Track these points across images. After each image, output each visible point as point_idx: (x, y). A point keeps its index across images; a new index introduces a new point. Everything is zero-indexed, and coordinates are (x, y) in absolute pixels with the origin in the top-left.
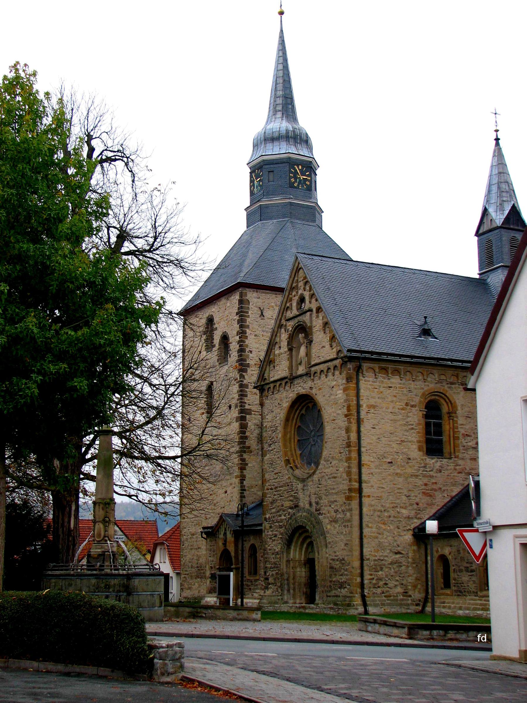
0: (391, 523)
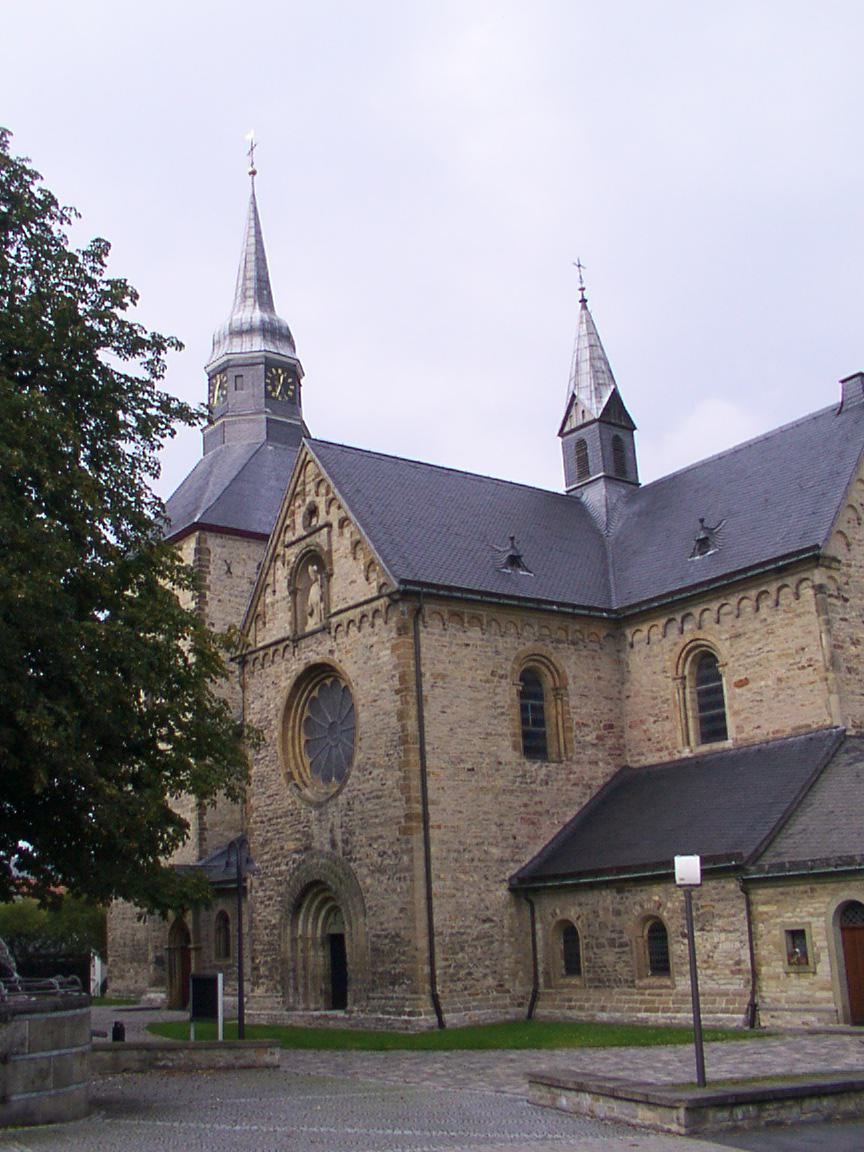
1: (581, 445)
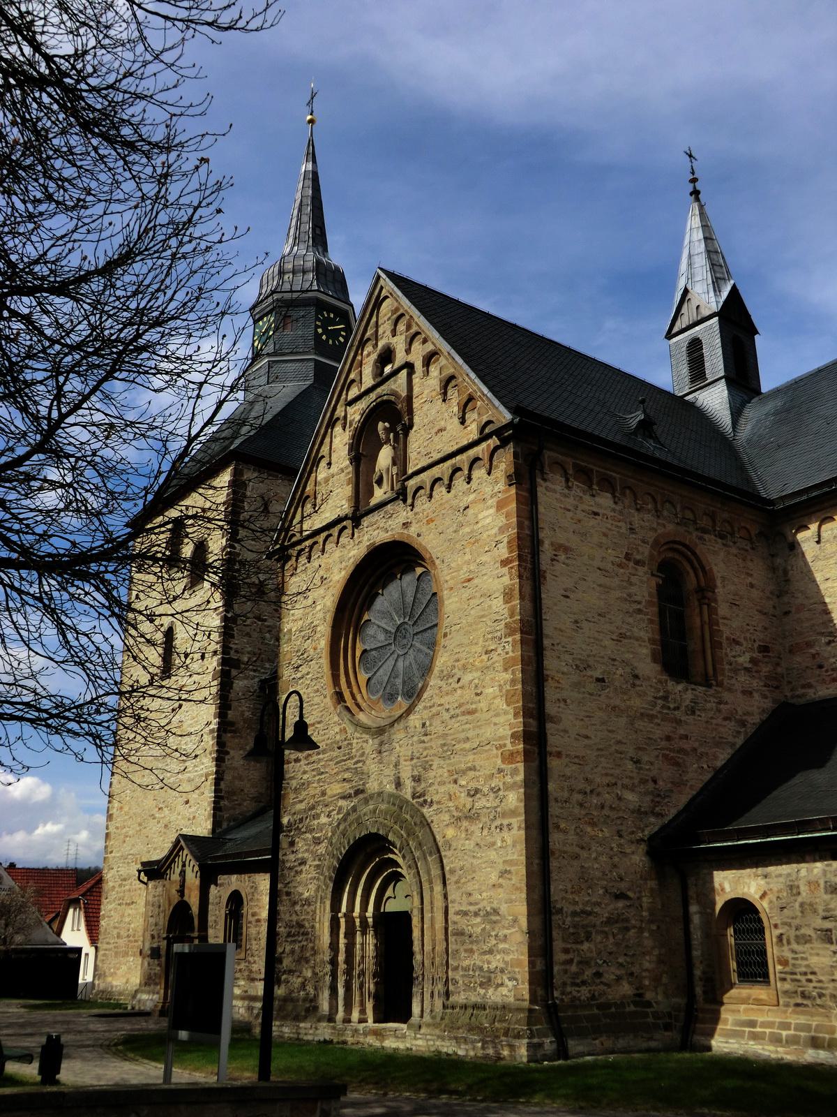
0: (605, 823)
1: (695, 347)
